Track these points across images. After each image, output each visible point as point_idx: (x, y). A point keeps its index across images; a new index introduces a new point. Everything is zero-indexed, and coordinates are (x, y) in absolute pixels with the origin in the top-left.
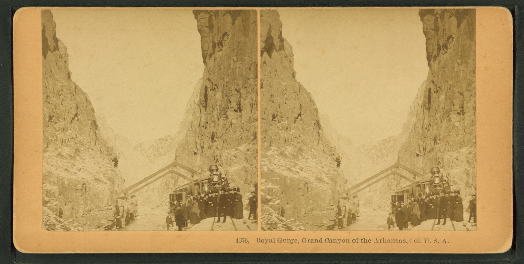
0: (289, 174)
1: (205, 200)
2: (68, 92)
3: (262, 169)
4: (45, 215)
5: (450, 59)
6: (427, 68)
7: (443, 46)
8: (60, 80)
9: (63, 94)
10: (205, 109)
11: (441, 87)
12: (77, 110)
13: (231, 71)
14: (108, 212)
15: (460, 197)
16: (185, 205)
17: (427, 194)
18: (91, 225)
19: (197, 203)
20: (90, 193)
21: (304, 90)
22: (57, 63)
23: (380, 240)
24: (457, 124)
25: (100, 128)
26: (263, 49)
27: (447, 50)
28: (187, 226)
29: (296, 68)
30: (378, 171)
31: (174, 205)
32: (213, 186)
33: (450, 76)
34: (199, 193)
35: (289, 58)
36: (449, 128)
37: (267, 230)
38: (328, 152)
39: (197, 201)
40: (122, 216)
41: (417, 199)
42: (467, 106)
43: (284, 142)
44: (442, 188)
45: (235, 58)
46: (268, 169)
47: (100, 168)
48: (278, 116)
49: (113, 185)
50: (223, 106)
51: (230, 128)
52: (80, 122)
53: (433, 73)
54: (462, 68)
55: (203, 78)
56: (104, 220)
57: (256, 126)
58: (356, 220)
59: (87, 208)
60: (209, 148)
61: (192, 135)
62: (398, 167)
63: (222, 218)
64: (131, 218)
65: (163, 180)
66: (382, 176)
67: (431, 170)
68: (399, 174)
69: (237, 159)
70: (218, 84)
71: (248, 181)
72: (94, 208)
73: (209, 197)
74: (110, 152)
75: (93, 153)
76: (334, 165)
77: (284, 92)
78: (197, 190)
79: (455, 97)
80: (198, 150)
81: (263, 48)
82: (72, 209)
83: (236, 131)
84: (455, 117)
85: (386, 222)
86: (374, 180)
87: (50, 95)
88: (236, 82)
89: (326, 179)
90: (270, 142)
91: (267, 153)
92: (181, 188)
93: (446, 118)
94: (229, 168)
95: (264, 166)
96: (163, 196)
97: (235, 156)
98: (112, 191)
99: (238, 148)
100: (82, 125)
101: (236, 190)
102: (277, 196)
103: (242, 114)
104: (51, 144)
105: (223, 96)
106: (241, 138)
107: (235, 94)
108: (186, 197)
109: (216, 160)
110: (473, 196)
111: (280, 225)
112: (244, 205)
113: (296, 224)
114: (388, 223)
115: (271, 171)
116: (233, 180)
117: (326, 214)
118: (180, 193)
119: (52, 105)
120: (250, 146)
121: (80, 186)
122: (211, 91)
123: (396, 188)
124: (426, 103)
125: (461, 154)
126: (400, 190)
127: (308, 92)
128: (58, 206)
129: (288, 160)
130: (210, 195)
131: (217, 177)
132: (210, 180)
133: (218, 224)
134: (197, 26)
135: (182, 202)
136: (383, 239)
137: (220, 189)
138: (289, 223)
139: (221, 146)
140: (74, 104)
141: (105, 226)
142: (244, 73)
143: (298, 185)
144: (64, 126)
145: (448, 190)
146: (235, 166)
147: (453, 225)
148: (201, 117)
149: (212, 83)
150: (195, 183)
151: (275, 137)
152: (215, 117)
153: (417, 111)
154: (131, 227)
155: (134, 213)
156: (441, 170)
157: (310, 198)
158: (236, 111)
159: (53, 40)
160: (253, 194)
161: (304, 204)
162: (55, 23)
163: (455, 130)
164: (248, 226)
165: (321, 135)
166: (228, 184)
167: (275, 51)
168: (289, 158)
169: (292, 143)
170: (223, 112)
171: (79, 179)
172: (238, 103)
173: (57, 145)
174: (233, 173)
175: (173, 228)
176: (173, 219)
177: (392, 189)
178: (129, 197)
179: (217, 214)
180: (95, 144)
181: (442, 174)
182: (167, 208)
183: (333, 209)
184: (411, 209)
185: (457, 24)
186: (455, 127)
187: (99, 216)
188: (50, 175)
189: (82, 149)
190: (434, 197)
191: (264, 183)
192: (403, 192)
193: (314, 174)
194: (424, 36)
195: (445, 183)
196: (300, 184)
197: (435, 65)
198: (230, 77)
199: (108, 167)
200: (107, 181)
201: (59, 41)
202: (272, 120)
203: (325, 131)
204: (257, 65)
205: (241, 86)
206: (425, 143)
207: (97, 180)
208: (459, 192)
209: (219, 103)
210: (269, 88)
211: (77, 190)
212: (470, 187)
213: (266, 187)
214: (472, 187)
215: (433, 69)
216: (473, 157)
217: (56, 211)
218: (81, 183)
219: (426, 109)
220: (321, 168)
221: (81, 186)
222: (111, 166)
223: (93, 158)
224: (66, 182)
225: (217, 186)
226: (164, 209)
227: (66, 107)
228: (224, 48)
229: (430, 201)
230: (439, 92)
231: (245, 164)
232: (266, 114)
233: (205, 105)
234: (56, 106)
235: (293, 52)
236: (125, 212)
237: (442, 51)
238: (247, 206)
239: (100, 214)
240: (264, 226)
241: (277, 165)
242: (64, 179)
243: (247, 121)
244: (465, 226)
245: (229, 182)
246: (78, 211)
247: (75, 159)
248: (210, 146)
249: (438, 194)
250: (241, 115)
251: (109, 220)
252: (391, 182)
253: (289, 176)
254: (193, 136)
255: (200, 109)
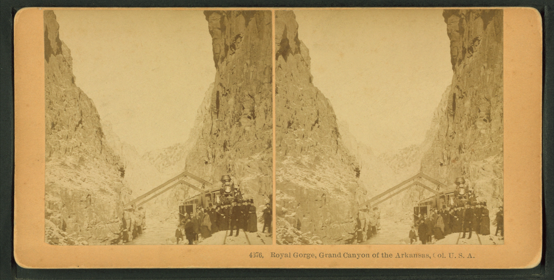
0: (306, 184)
1: (217, 213)
2: (72, 97)
3: (277, 180)
4: (48, 228)
5: (476, 63)
6: (452, 73)
7: (469, 49)
8: (64, 84)
9: (67, 100)
10: (216, 115)
11: (466, 93)
12: (81, 117)
13: (244, 76)
14: (114, 225)
15: (486, 209)
16: (196, 217)
17: (451, 206)
18: (96, 239)
19: (208, 216)
20: (95, 204)
21: (322, 95)
22: (60, 67)
23: (402, 254)
24: (483, 131)
25: (106, 135)
26: (278, 52)
27: (473, 53)
28: (198, 240)
29: (313, 72)
30: (400, 182)
31: (184, 217)
32: (225, 197)
33: (476, 80)
34: (211, 205)
35: (306, 62)
36: (475, 136)
37: (282, 243)
38: (347, 162)
39: (208, 213)
40: (130, 229)
41: (441, 211)
42: (258, 110)
43: (301, 150)
44: (467, 200)
45: (248, 62)
46: (283, 179)
47: (106, 178)
48: (294, 123)
49: (120, 196)
50: (236, 112)
51: (243, 136)
52: (85, 130)
53: (458, 78)
54: (489, 72)
55: (215, 83)
56: (110, 233)
57: (271, 133)
58: (142, 233)
59: (92, 221)
60: (221, 157)
61: (203, 144)
62: (420, 178)
63: (235, 232)
64: (138, 231)
65: (172, 191)
66: (404, 186)
67: (222, 178)
68: (421, 185)
69: (251, 169)
70: (231, 89)
71: (262, 192)
72: (99, 220)
73: (221, 209)
74: (117, 161)
75: (98, 162)
76: (118, 175)
77: (300, 98)
78: (208, 201)
79: (244, 99)
80: (209, 159)
81: (278, 51)
82: (77, 222)
83: (249, 138)
84: (481, 124)
85: (408, 235)
86: (395, 191)
87: (53, 100)
88: (249, 87)
89: (345, 190)
90: (286, 151)
91: (282, 163)
92: (191, 199)
93: (471, 125)
94: (242, 178)
95: (279, 176)
96: (172, 208)
97: (483, 168)
98: (118, 202)
99: (251, 156)
100: (87, 133)
101: (250, 202)
102: (293, 208)
103: (256, 121)
104: (54, 153)
105: (236, 102)
106: (255, 146)
107: (249, 100)
108: (197, 208)
109: (228, 169)
110: (501, 208)
111: (295, 239)
112: (258, 218)
113: (313, 237)
114: (410, 236)
115: (286, 182)
116: (247, 191)
117: (345, 227)
118: (425, 206)
119: (55, 111)
120: (265, 155)
121: (84, 198)
122: (223, 96)
123: (418, 200)
124: (451, 109)
125: (487, 163)
126: (422, 202)
127: (89, 97)
128: (62, 218)
129: (304, 169)
130: (222, 207)
131: (230, 187)
132: (222, 191)
133: (231, 237)
134: (446, 30)
135: (192, 215)
136: (405, 254)
137: (233, 200)
138: (306, 236)
139: (234, 155)
140: (78, 110)
141: (111, 240)
142: (258, 78)
143: (315, 196)
144: (67, 134)
145: (474, 202)
146: (248, 176)
147: (479, 238)
148: (212, 124)
149: (224, 88)
150: (206, 195)
151: (291, 146)
152: (228, 124)
153: (441, 118)
154: (139, 240)
155: (142, 226)
156: (466, 180)
157: (328, 210)
158: (249, 117)
159: (56, 43)
160: (268, 205)
161: (321, 216)
162: (58, 25)
163: (481, 138)
164: (262, 240)
165: (339, 144)
166: (241, 195)
167: (290, 54)
168: (306, 167)
169: (309, 151)
170: (236, 119)
171: (83, 190)
172: (488, 113)
173: (60, 154)
174: (247, 183)
175: (183, 241)
176: (183, 232)
177: (415, 200)
178: (137, 209)
179: (230, 227)
180: (101, 153)
181: (467, 184)
182: (176, 220)
183: (352, 221)
184: (435, 222)
185: (483, 26)
186: (246, 132)
187: (105, 229)
188: (53, 186)
189: (87, 158)
190: (459, 209)
191: (279, 194)
192: (426, 203)
193: (332, 185)
194: (449, 38)
195: (470, 195)
196: (318, 195)
197: (460, 69)
198: (243, 81)
199: (114, 177)
200: (114, 192)
201: (301, 43)
202: (288, 127)
203: (344, 139)
204: (271, 69)
205: (254, 91)
206: (449, 152)
207: (103, 191)
208: (485, 204)
209: (231, 109)
210: (284, 93)
211: (82, 201)
212: (497, 198)
213: (281, 198)
214: (499, 198)
215: (458, 73)
216: (500, 166)
217: (59, 223)
218: (86, 194)
219: (450, 115)
220: (340, 178)
221: (85, 198)
222: (352, 176)
223: (99, 167)
224: (70, 194)
225: (230, 197)
226: (173, 222)
227: (70, 113)
228: (237, 51)
229: (455, 213)
230: (464, 98)
231: (259, 174)
232: (281, 121)
233: (216, 112)
234: (59, 113)
235: (310, 55)
236: (132, 225)
237: (467, 55)
238: (261, 218)
239: (106, 227)
240: (279, 240)
241: (293, 175)
242: (68, 190)
243: (497, 131)
244: (491, 239)
245: (242, 194)
246: (83, 224)
247: (80, 169)
248: (222, 155)
249: (463, 206)
250: (255, 122)
251: (116, 234)
252: (179, 192)
253: (305, 186)
254: (204, 144)
255: (212, 116)
